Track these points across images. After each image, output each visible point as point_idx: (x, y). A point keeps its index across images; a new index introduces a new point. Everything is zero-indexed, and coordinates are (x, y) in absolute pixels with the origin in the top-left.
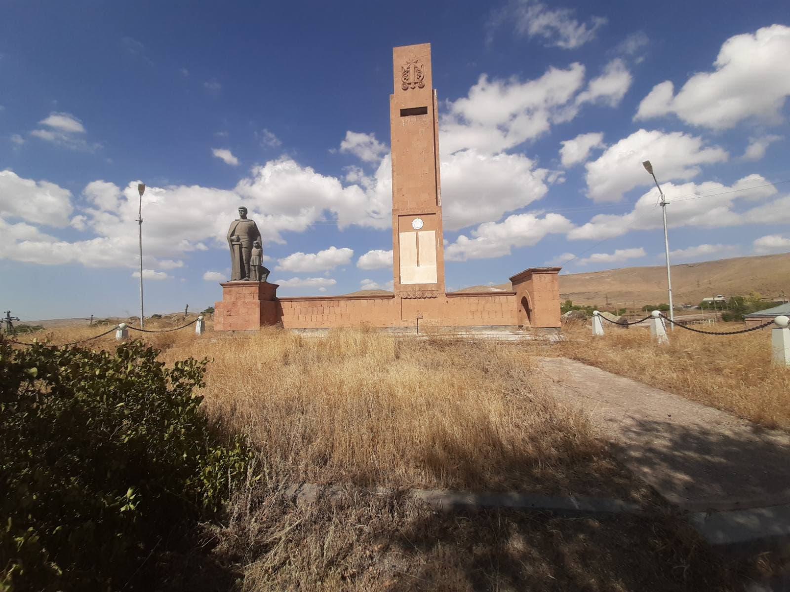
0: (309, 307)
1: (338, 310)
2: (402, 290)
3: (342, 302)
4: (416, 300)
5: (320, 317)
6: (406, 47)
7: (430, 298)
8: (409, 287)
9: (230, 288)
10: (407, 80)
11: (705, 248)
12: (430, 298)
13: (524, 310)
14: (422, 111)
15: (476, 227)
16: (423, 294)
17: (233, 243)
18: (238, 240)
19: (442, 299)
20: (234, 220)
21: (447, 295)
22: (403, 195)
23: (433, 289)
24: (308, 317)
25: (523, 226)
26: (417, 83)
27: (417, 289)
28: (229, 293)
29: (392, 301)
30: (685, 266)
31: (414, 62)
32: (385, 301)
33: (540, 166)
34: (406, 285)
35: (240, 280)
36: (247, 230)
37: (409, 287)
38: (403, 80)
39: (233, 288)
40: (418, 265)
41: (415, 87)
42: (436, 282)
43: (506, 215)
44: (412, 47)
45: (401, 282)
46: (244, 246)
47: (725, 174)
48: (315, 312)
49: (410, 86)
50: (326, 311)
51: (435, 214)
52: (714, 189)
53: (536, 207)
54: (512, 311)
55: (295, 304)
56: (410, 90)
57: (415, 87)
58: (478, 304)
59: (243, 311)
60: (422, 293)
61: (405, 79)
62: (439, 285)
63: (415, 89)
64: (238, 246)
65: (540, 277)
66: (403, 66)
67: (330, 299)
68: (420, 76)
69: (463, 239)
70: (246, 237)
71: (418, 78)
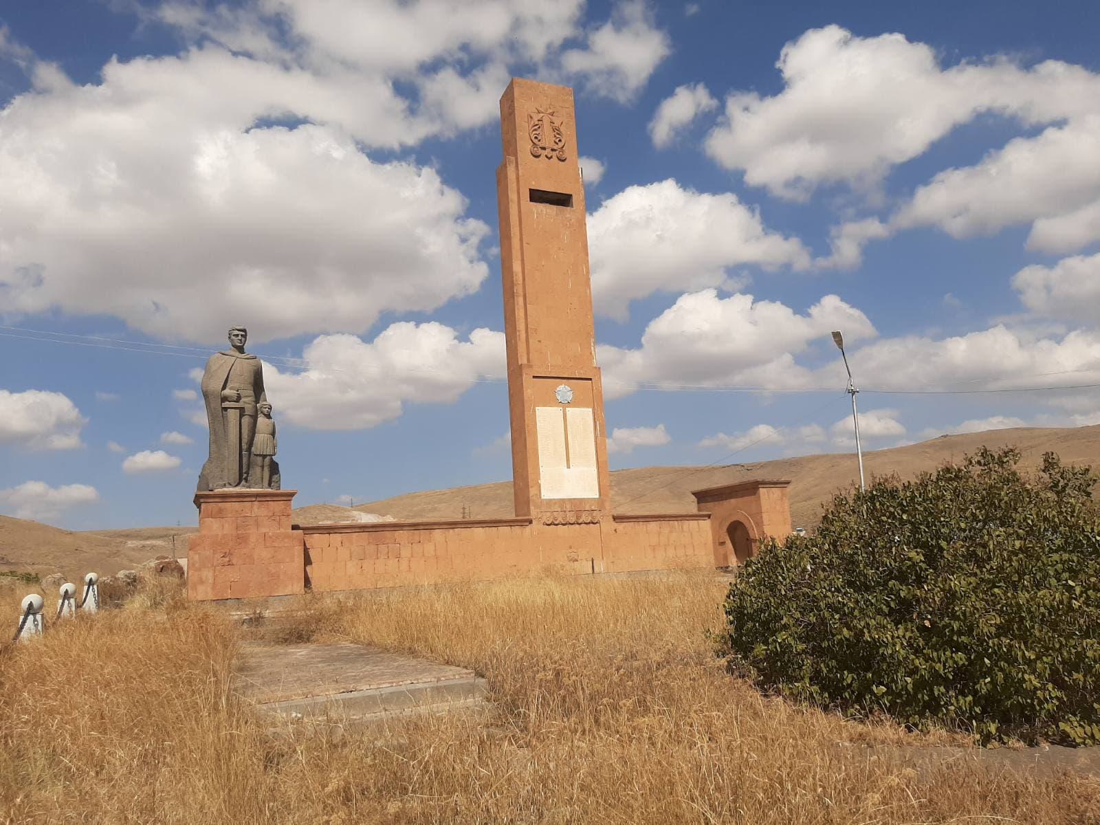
1: (429, 548)
2: (543, 509)
3: (438, 534)
4: (566, 526)
5: (392, 562)
7: (589, 523)
8: (555, 503)
9: (220, 504)
10: (539, 141)
11: (763, 432)
12: (589, 523)
13: (730, 541)
15: (307, 339)
16: (578, 517)
17: (226, 404)
18: (238, 399)
19: (608, 526)
21: (615, 518)
22: (540, 341)
23: (593, 508)
26: (556, 150)
29: (528, 529)
31: (549, 114)
32: (517, 529)
34: (551, 500)
37: (555, 503)
38: (533, 139)
39: (228, 505)
40: (569, 467)
41: (551, 157)
42: (598, 497)
43: (386, 319)
45: (542, 495)
47: (794, 291)
50: (405, 553)
51: (534, 377)
52: (776, 314)
54: (706, 544)
55: (336, 538)
56: (543, 158)
57: (551, 157)
58: (659, 533)
59: (263, 553)
60: (575, 514)
61: (536, 138)
62: (601, 501)
65: (768, 492)
66: (532, 115)
67: (415, 526)
68: (560, 141)
70: (252, 393)
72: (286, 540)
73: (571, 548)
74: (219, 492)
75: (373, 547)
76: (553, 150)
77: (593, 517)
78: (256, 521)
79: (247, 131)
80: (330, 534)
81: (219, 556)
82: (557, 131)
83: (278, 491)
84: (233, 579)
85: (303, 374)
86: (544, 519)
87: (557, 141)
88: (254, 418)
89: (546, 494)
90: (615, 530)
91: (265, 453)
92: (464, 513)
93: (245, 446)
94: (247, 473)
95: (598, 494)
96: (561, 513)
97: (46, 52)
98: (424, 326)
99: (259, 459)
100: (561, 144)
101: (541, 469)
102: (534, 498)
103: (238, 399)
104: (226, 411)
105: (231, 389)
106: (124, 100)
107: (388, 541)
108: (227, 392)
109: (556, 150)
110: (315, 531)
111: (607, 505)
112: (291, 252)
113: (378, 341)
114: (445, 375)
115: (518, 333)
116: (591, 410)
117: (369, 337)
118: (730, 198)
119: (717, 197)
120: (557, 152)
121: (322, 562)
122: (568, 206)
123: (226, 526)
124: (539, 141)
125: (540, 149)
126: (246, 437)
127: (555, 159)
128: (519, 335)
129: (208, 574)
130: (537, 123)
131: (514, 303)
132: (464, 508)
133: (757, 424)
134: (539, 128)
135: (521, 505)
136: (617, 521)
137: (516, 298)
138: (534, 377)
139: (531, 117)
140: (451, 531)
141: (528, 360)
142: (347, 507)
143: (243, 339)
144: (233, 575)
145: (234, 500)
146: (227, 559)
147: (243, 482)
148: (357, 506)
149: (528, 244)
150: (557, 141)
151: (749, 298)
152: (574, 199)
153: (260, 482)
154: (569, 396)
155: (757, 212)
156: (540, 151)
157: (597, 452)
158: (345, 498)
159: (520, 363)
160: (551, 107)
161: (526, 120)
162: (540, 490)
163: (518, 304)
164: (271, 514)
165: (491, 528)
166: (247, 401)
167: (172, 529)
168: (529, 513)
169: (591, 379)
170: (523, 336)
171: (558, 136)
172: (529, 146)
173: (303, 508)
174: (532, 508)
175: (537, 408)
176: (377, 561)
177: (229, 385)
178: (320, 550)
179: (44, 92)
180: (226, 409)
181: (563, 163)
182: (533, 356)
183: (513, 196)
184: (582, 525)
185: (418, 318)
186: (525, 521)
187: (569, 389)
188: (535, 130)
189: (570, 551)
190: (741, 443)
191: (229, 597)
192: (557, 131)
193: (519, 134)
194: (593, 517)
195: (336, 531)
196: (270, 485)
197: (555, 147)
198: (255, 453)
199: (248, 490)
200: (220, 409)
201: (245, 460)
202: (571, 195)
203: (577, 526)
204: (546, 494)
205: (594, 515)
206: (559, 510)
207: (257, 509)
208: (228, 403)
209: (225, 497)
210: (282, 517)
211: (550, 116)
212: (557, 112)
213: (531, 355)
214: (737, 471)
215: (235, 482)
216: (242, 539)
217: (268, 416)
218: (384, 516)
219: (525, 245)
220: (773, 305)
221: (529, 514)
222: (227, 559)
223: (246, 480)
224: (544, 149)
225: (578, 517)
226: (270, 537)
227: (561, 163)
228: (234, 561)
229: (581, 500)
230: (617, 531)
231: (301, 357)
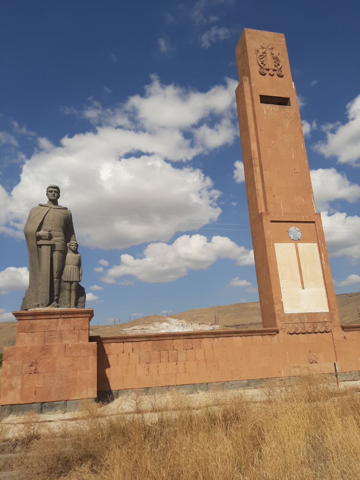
0: (154, 350)
1: (200, 353)
4: (306, 335)
6: (259, 31)
7: (323, 332)
8: (296, 317)
9: (32, 321)
12: (323, 332)
14: (283, 102)
17: (40, 242)
18: (50, 237)
19: (339, 334)
20: (37, 205)
21: (343, 328)
23: (326, 320)
24: (152, 366)
25: (193, 247)
26: (276, 70)
27: (306, 320)
28: (30, 330)
29: (276, 338)
30: (345, 296)
31: (270, 49)
32: (267, 338)
33: (215, 187)
34: (291, 314)
35: (47, 306)
36: (62, 224)
37: (296, 317)
38: (260, 63)
43: (179, 234)
44: (267, 33)
46: (57, 248)
48: (164, 360)
49: (268, 72)
50: (182, 357)
51: (271, 221)
53: (208, 231)
55: (128, 346)
56: (267, 76)
61: (262, 63)
62: (331, 314)
63: (273, 76)
64: (50, 247)
68: (278, 65)
69: (126, 258)
70: (61, 234)
71: (275, 66)
72: (83, 351)
73: (310, 352)
74: (32, 311)
75: (156, 352)
76: (274, 70)
77: (326, 327)
78: (61, 334)
79: (120, 158)
80: (123, 342)
81: (26, 366)
82: (276, 59)
83: (83, 310)
84: (37, 386)
85: (144, 259)
86: (288, 330)
87: (277, 64)
88: (64, 253)
89: (288, 309)
90: (345, 337)
91: (71, 280)
92: (215, 318)
93: (55, 275)
94: (58, 295)
95: (328, 309)
96: (301, 324)
97: (42, 134)
98: (193, 236)
99: (68, 285)
100: (279, 67)
101: (282, 290)
102: (279, 312)
103: (50, 237)
104: (41, 247)
105: (44, 230)
106: (70, 152)
107: (167, 348)
108: (41, 233)
109: (276, 70)
110: (112, 341)
111: (336, 317)
112: (137, 208)
113: (174, 244)
114: (202, 257)
115: (257, 192)
116: (316, 244)
117: (171, 242)
118: (333, 170)
119: (325, 170)
120: (277, 71)
121: (118, 365)
122: (287, 105)
123: (36, 339)
124: (265, 65)
125: (265, 70)
126: (57, 267)
127: (276, 76)
128: (258, 193)
129: (17, 381)
130: (262, 54)
131: (253, 171)
132: (215, 316)
133: (350, 275)
134: (264, 57)
135: (267, 319)
136: (345, 330)
137: (254, 167)
138: (271, 221)
139: (258, 51)
140: (216, 339)
141: (266, 210)
142: (165, 316)
143: (56, 195)
144: (38, 382)
145: (42, 317)
146: (33, 368)
147: (54, 303)
148: (169, 316)
149: (261, 130)
150: (277, 64)
151: (344, 214)
152: (291, 100)
153: (68, 303)
154: (299, 235)
155: (345, 176)
156: (265, 71)
157: (324, 276)
158: (164, 312)
159: (260, 212)
160: (271, 45)
161: (255, 53)
162: (283, 306)
163: (256, 172)
164: (72, 328)
165: (246, 337)
166: (58, 240)
167: (95, 326)
168: (275, 325)
169: (314, 222)
170: (261, 193)
171: (277, 62)
172: (257, 68)
173: (101, 323)
174: (278, 321)
175: (275, 244)
176: (160, 364)
177: (44, 227)
178: (116, 356)
179: (41, 150)
180: (40, 246)
181: (281, 78)
182: (270, 207)
183: (248, 101)
184: (318, 334)
185: (190, 233)
186: (274, 331)
187: (299, 230)
188: (261, 59)
189: (311, 354)
190: (344, 283)
191: (34, 401)
192: (276, 59)
193: (250, 62)
194: (326, 327)
195: (129, 340)
196: (76, 305)
197: (276, 68)
198: (64, 280)
199: (56, 309)
200: (36, 246)
201: (56, 285)
202: (289, 98)
203: (314, 334)
204: (288, 309)
205: (327, 325)
206: (299, 321)
207: (62, 325)
208: (42, 241)
209: (35, 315)
210: (81, 331)
211: (271, 50)
212: (275, 48)
213: (268, 205)
214: (344, 297)
215: (46, 303)
216: (46, 350)
217: (76, 252)
218: (181, 320)
219: (259, 131)
220: (353, 217)
221: (276, 326)
222: (33, 368)
223: (57, 301)
224: (268, 70)
225: (315, 328)
226: (70, 348)
227: (280, 78)
228: (40, 369)
229: (316, 314)
230: (346, 338)
231: (143, 254)
